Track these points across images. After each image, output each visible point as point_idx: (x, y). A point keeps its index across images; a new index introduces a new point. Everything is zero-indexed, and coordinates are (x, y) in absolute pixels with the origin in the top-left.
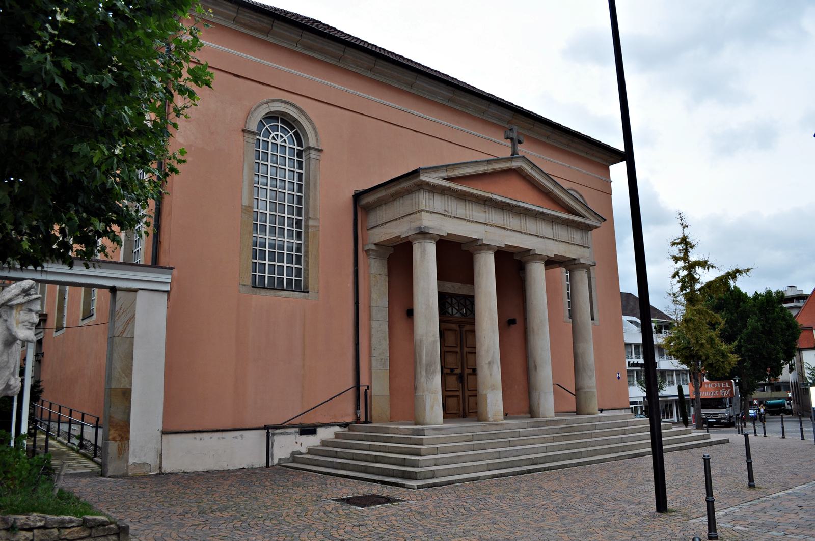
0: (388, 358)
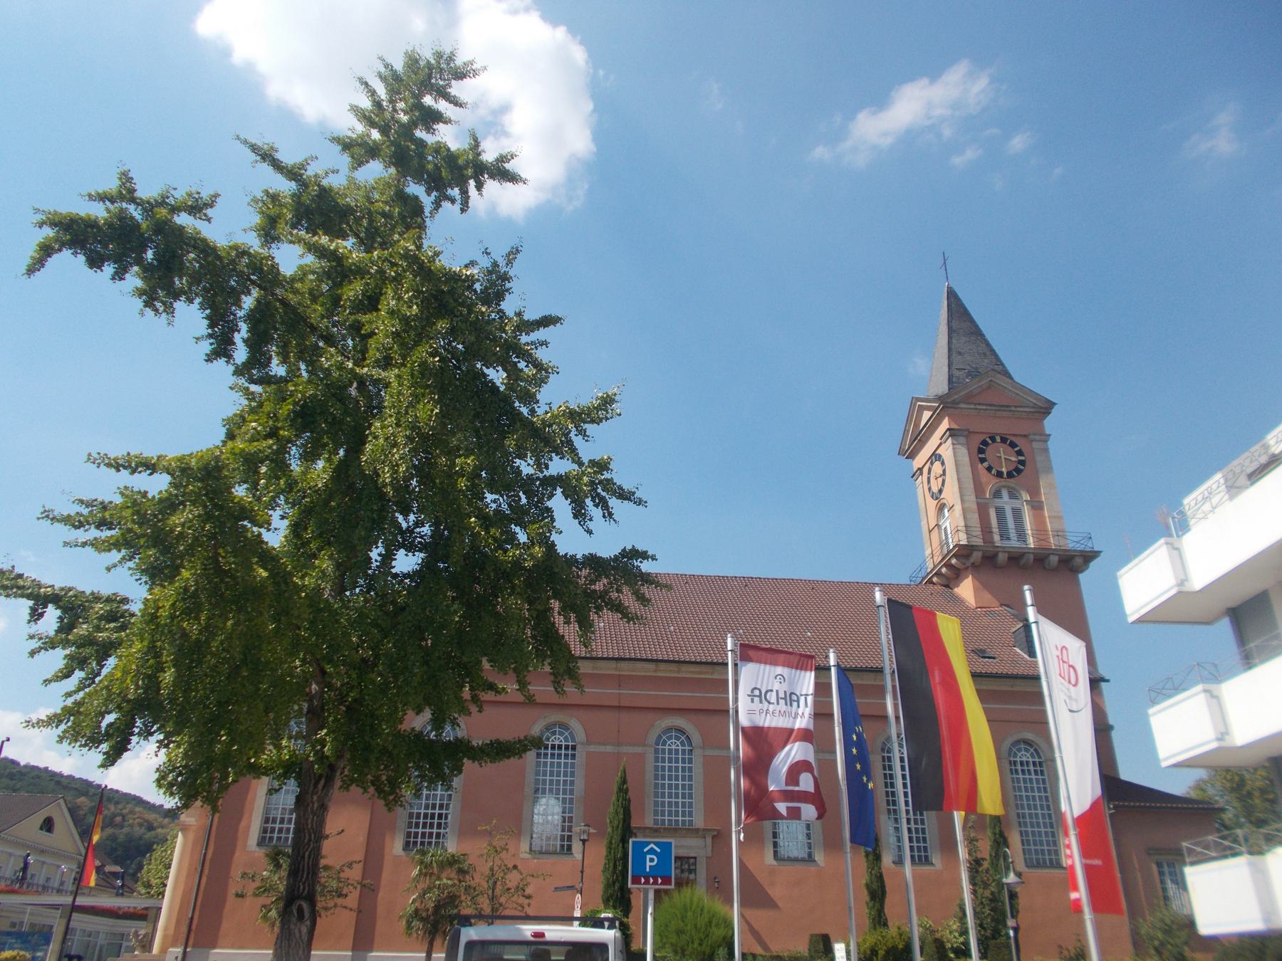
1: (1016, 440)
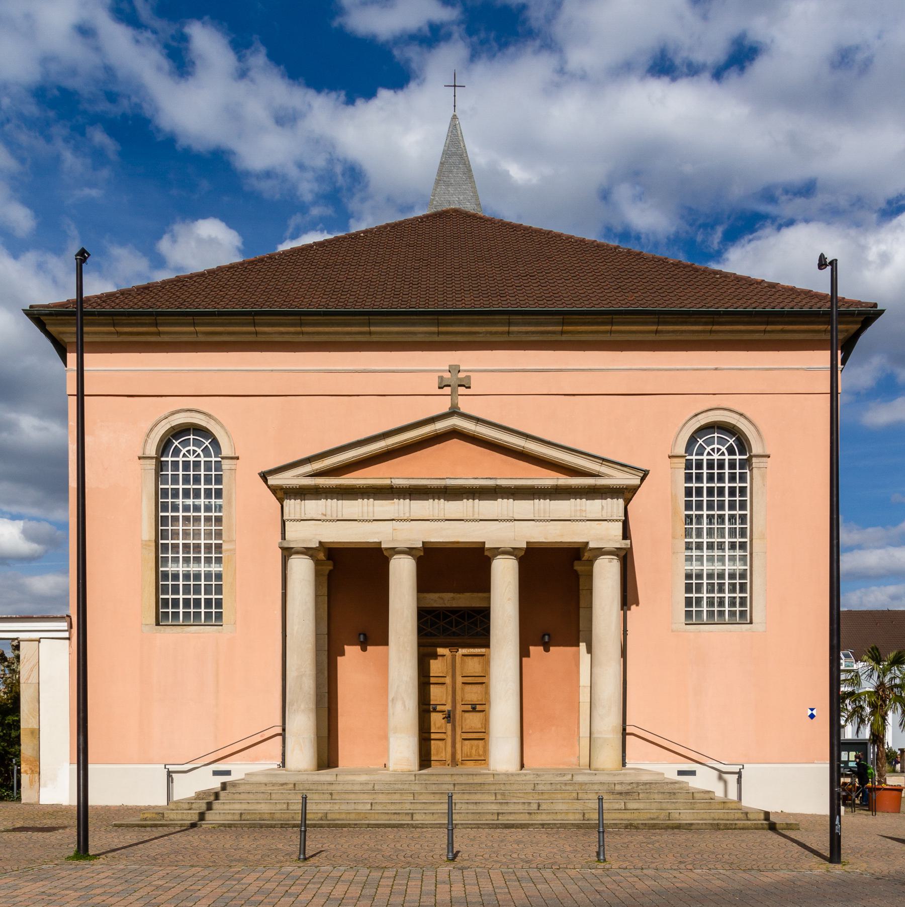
0: (327, 694)
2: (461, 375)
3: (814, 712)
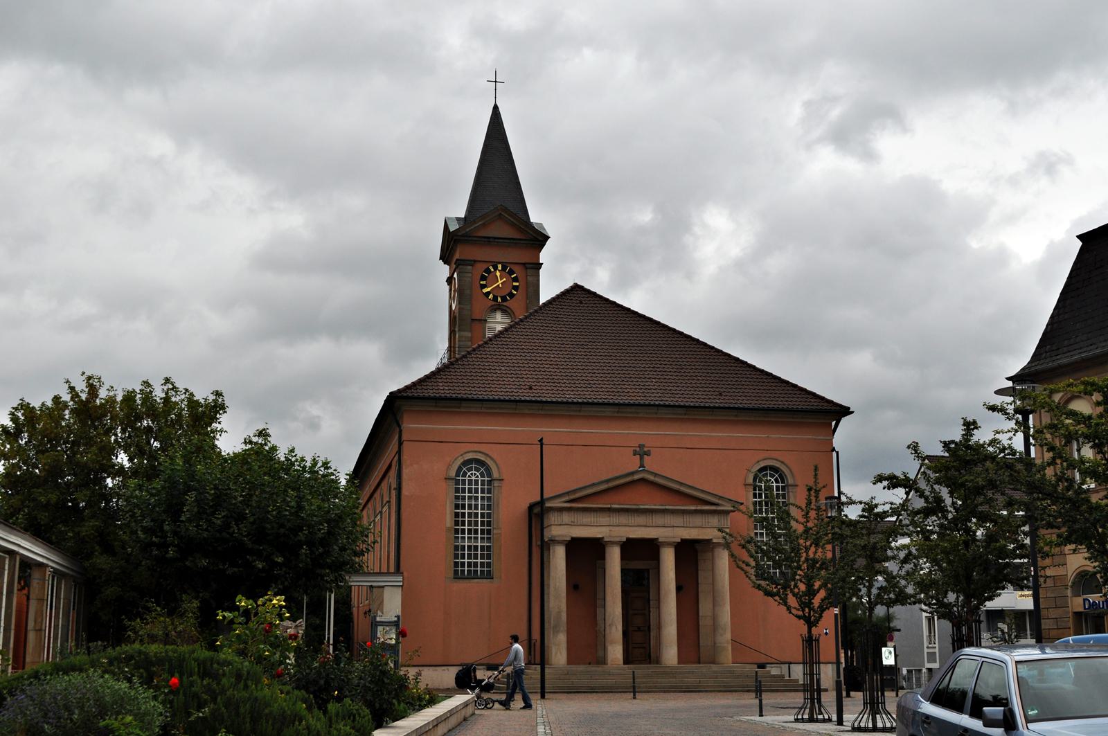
1: (515, 268)
2: (646, 449)
3: (827, 631)
